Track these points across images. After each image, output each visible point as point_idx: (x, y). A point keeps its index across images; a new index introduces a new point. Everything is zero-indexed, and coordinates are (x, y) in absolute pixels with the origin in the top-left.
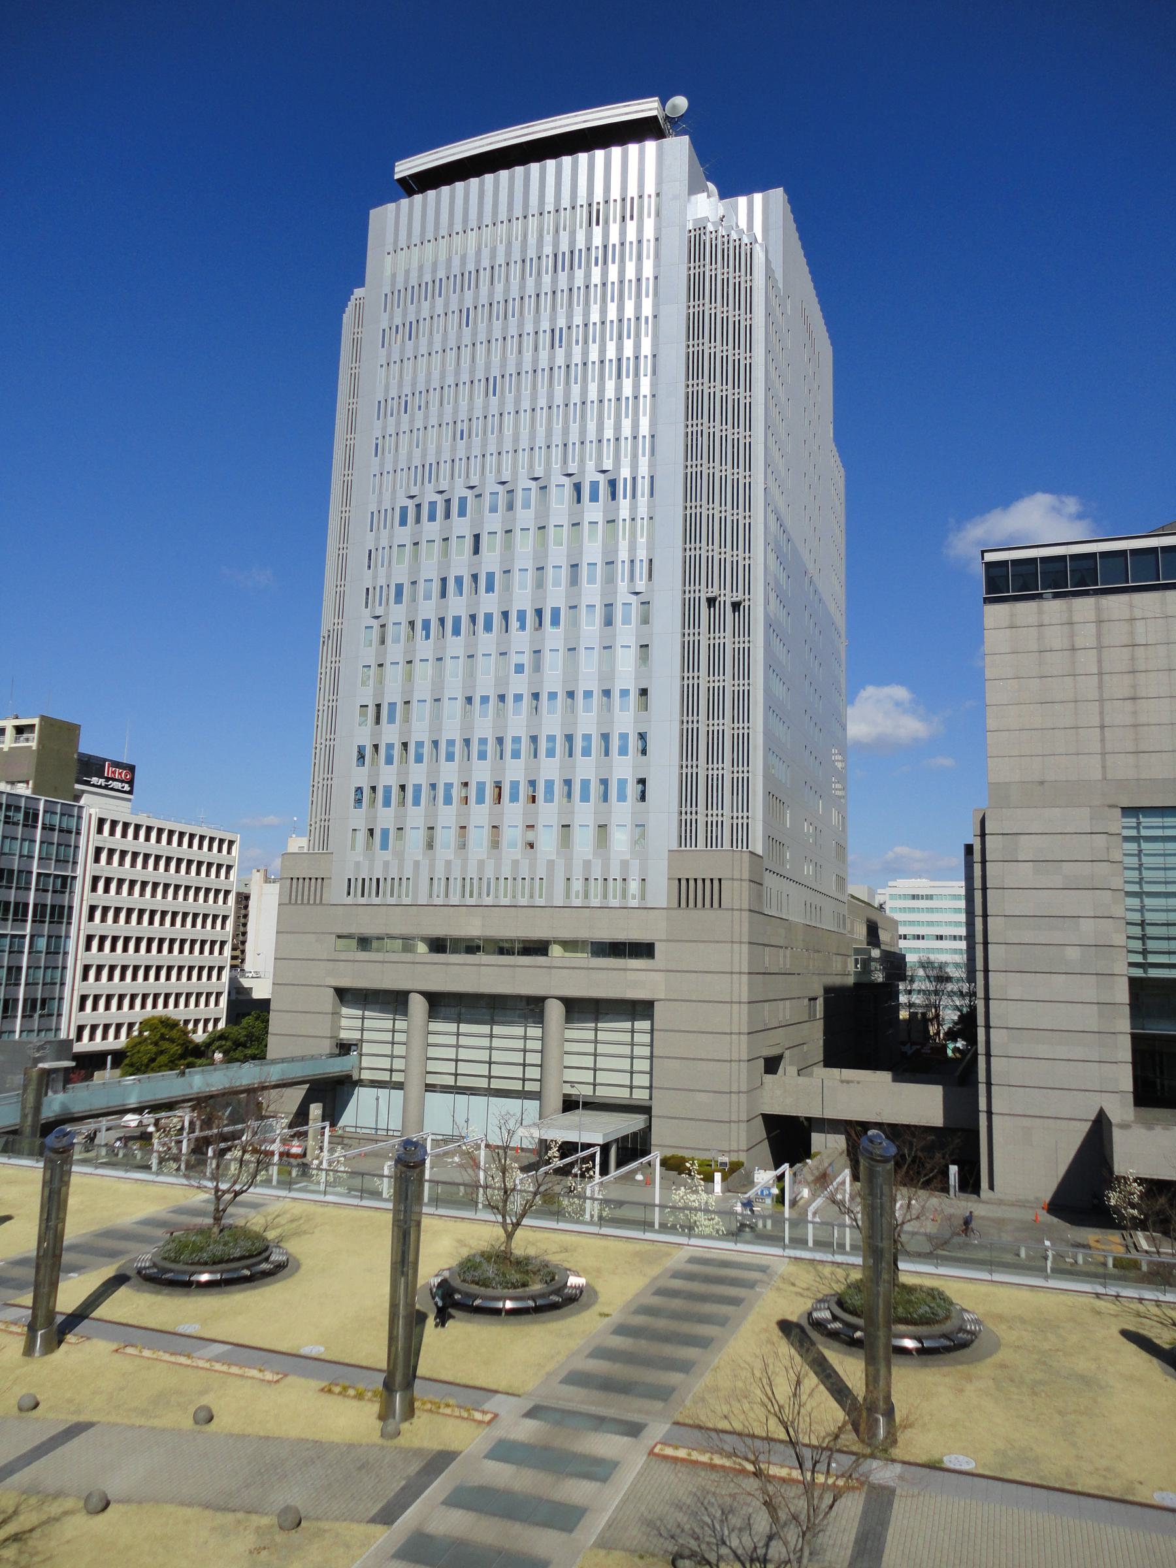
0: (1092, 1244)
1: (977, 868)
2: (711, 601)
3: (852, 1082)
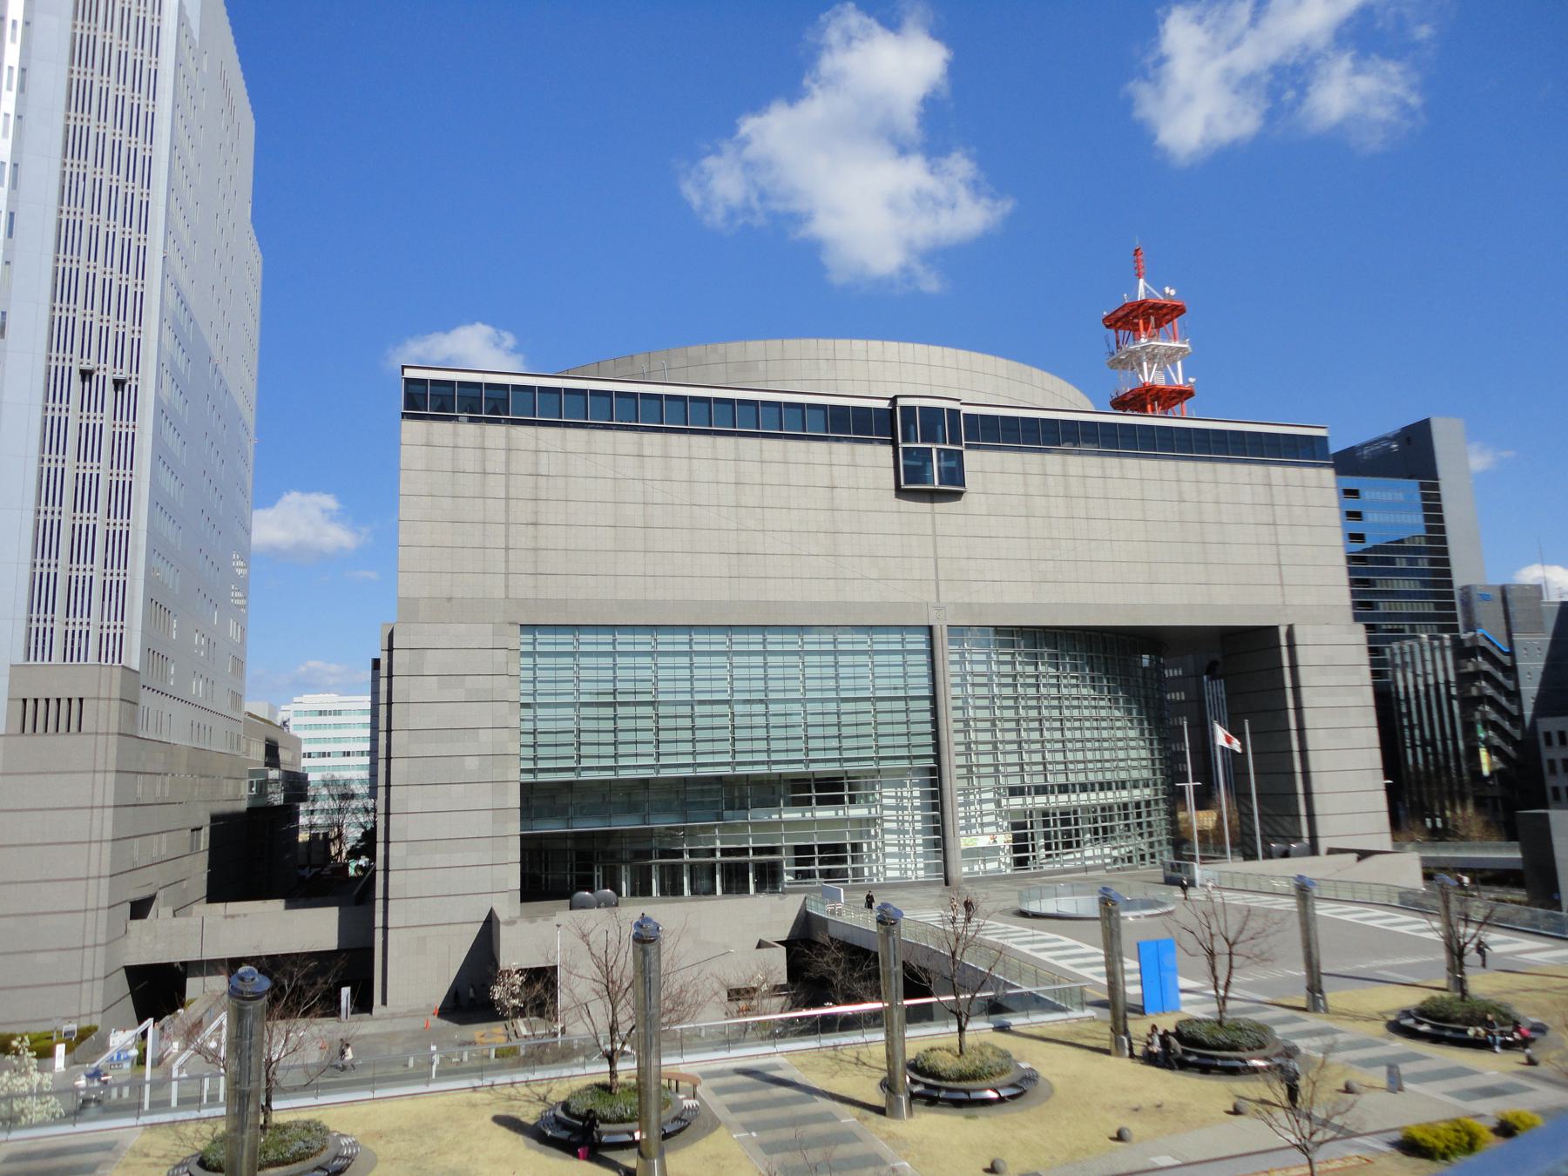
0: (478, 1039)
1: (383, 683)
2: (86, 375)
3: (238, 916)
